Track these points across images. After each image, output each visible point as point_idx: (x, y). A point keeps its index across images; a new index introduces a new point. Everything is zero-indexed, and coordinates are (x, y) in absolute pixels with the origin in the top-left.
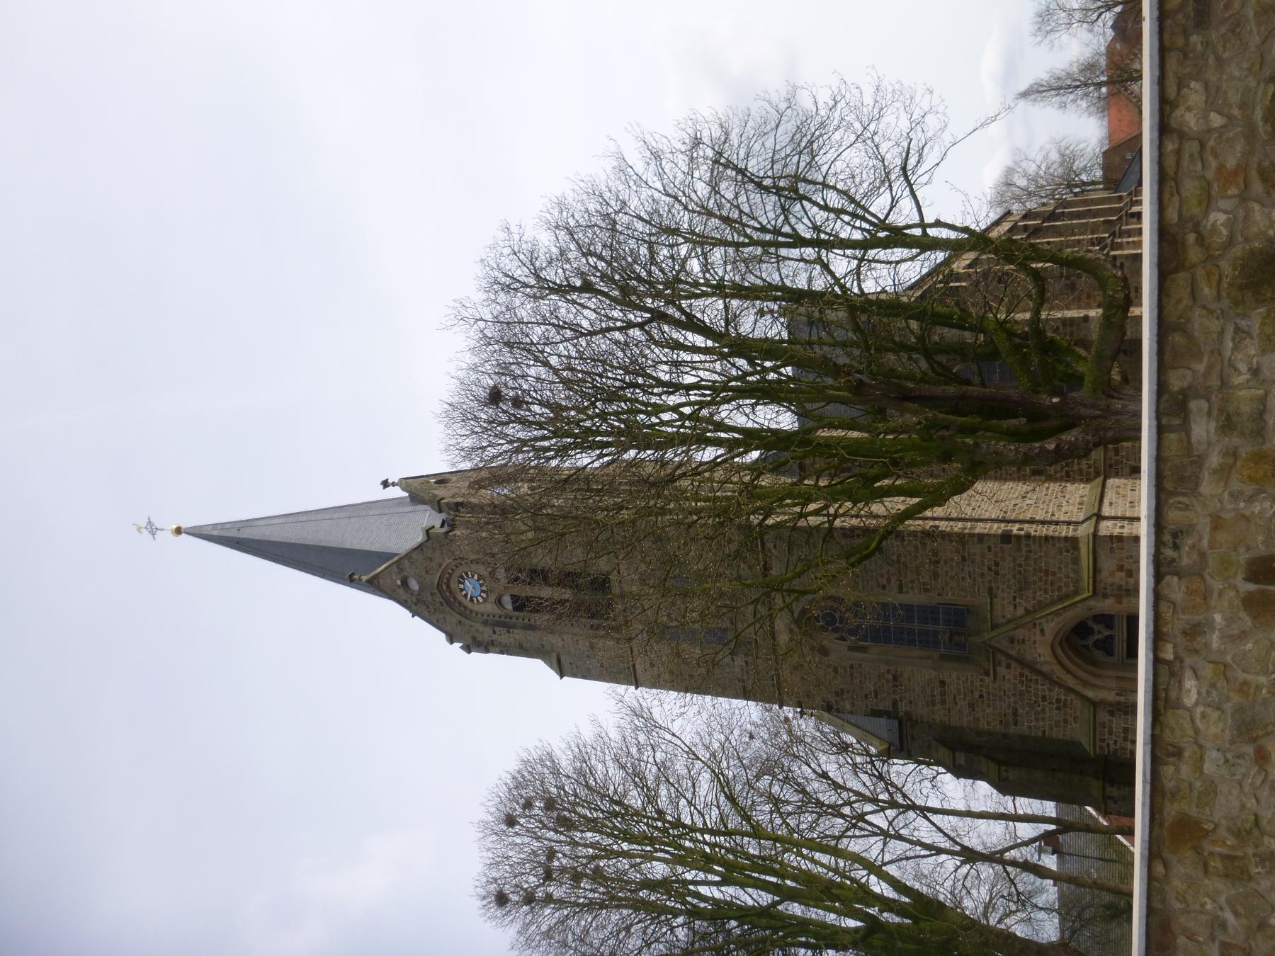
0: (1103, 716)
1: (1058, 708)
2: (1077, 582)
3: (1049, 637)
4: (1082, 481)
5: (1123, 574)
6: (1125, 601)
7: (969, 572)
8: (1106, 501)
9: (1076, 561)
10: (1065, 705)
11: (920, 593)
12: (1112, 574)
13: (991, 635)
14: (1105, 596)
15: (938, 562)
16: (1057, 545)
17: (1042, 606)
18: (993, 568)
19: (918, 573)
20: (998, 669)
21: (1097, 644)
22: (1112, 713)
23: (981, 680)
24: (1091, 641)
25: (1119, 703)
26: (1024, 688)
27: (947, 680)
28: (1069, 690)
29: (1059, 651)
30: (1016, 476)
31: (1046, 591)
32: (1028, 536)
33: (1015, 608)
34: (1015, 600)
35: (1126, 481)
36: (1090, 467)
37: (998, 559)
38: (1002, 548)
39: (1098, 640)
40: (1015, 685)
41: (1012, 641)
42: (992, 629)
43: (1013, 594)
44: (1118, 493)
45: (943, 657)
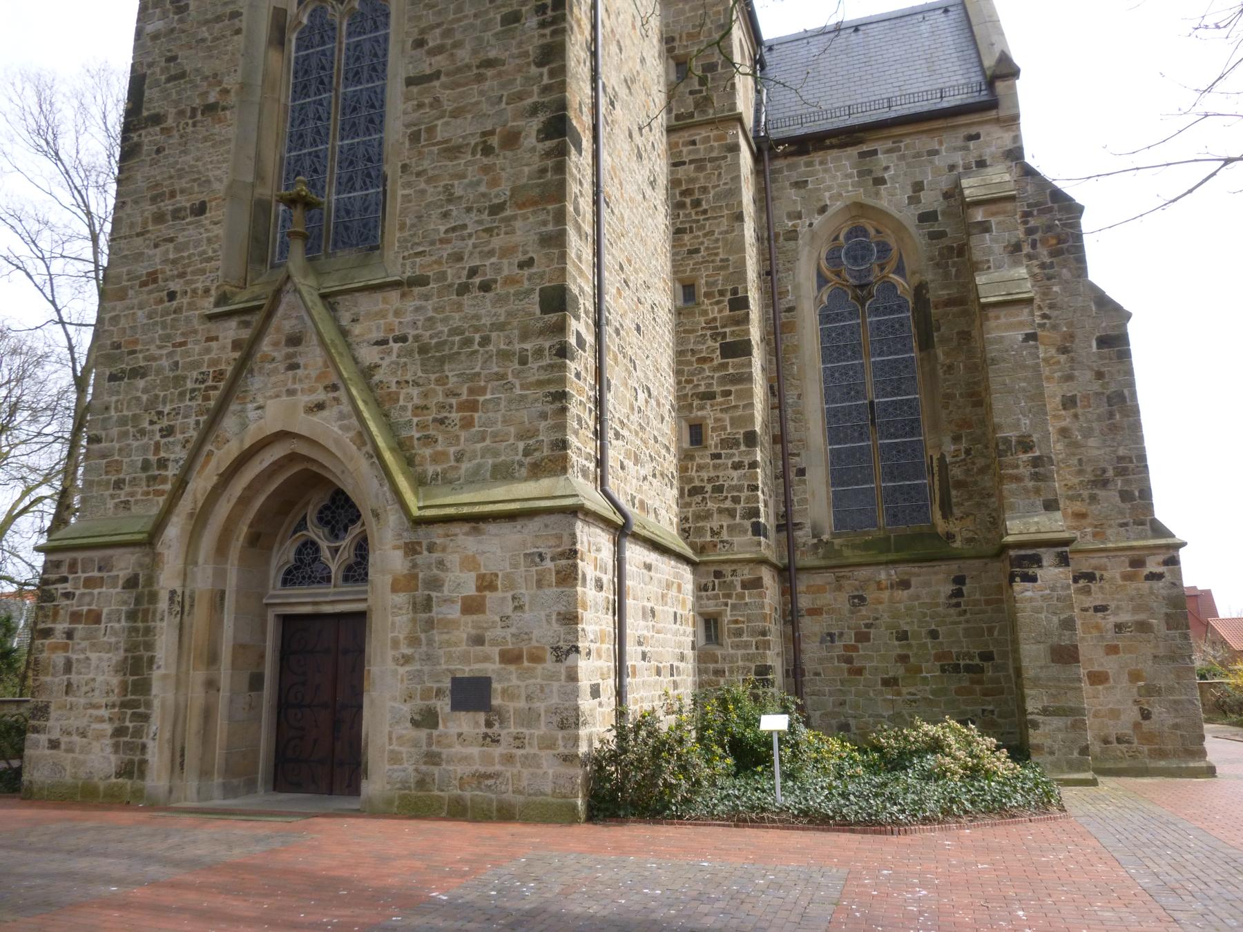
0: (125, 563)
1: (146, 466)
2: (447, 480)
3: (302, 424)
4: (685, 519)
5: (470, 590)
6: (401, 598)
7: (464, 226)
8: (653, 557)
9: (503, 473)
10: (152, 479)
11: (407, 126)
12: (469, 563)
13: (304, 290)
14: (411, 549)
15: (487, 150)
16: (543, 425)
17: (383, 404)
18: (477, 280)
19: (456, 114)
20: (233, 323)
21: (309, 547)
22: (131, 583)
23: (207, 291)
24: (315, 533)
25: (153, 597)
26: (190, 385)
27: (205, 220)
28: (182, 483)
29: (296, 469)
30: (688, 389)
31: (420, 409)
32: (563, 352)
33: (378, 343)
34: (396, 340)
35: (689, 605)
36: (713, 533)
37: (499, 289)
38: (528, 292)
39: (318, 550)
40: (195, 365)
41: (295, 340)
42: (324, 297)
43: (412, 333)
44: (669, 586)
45: (261, 208)
